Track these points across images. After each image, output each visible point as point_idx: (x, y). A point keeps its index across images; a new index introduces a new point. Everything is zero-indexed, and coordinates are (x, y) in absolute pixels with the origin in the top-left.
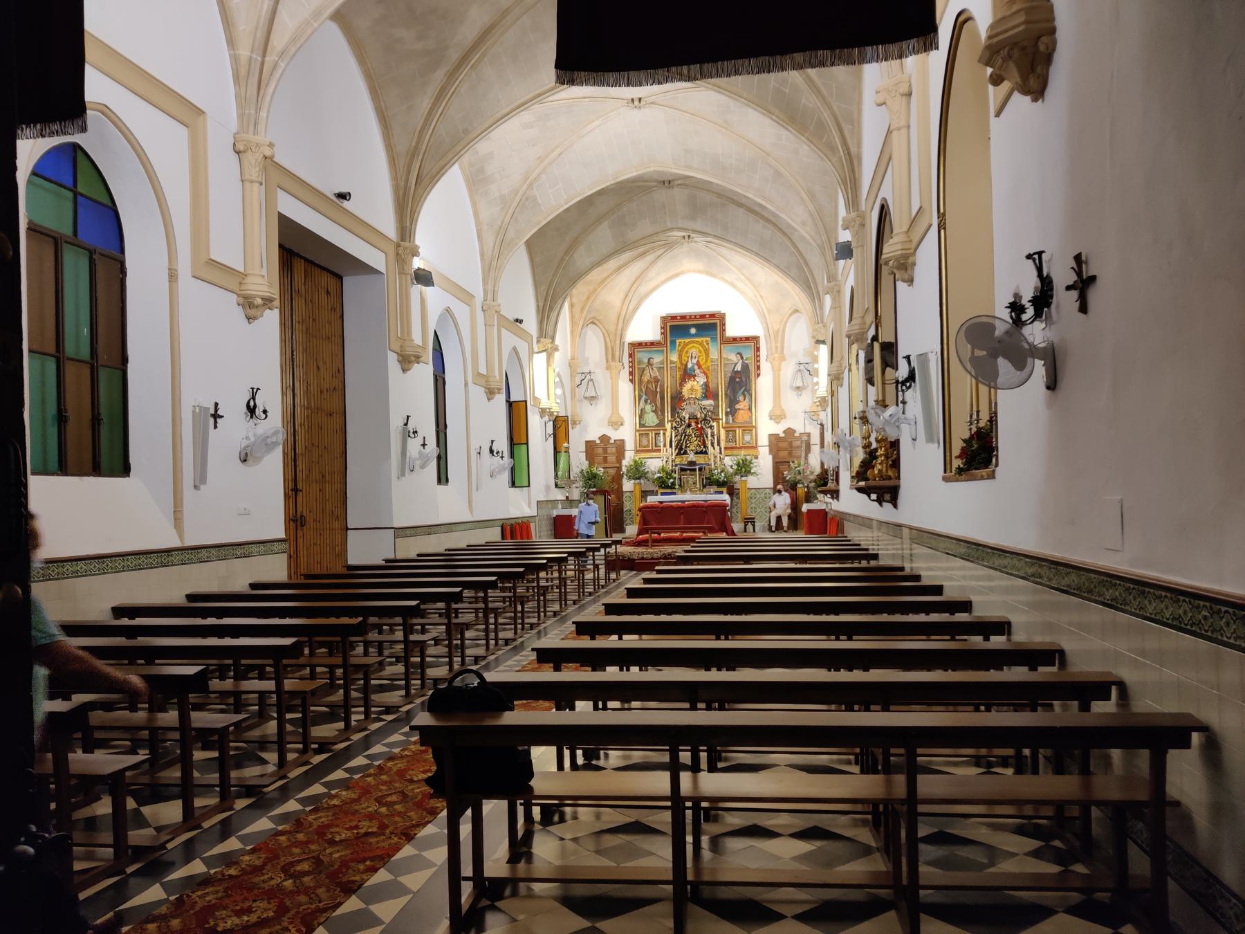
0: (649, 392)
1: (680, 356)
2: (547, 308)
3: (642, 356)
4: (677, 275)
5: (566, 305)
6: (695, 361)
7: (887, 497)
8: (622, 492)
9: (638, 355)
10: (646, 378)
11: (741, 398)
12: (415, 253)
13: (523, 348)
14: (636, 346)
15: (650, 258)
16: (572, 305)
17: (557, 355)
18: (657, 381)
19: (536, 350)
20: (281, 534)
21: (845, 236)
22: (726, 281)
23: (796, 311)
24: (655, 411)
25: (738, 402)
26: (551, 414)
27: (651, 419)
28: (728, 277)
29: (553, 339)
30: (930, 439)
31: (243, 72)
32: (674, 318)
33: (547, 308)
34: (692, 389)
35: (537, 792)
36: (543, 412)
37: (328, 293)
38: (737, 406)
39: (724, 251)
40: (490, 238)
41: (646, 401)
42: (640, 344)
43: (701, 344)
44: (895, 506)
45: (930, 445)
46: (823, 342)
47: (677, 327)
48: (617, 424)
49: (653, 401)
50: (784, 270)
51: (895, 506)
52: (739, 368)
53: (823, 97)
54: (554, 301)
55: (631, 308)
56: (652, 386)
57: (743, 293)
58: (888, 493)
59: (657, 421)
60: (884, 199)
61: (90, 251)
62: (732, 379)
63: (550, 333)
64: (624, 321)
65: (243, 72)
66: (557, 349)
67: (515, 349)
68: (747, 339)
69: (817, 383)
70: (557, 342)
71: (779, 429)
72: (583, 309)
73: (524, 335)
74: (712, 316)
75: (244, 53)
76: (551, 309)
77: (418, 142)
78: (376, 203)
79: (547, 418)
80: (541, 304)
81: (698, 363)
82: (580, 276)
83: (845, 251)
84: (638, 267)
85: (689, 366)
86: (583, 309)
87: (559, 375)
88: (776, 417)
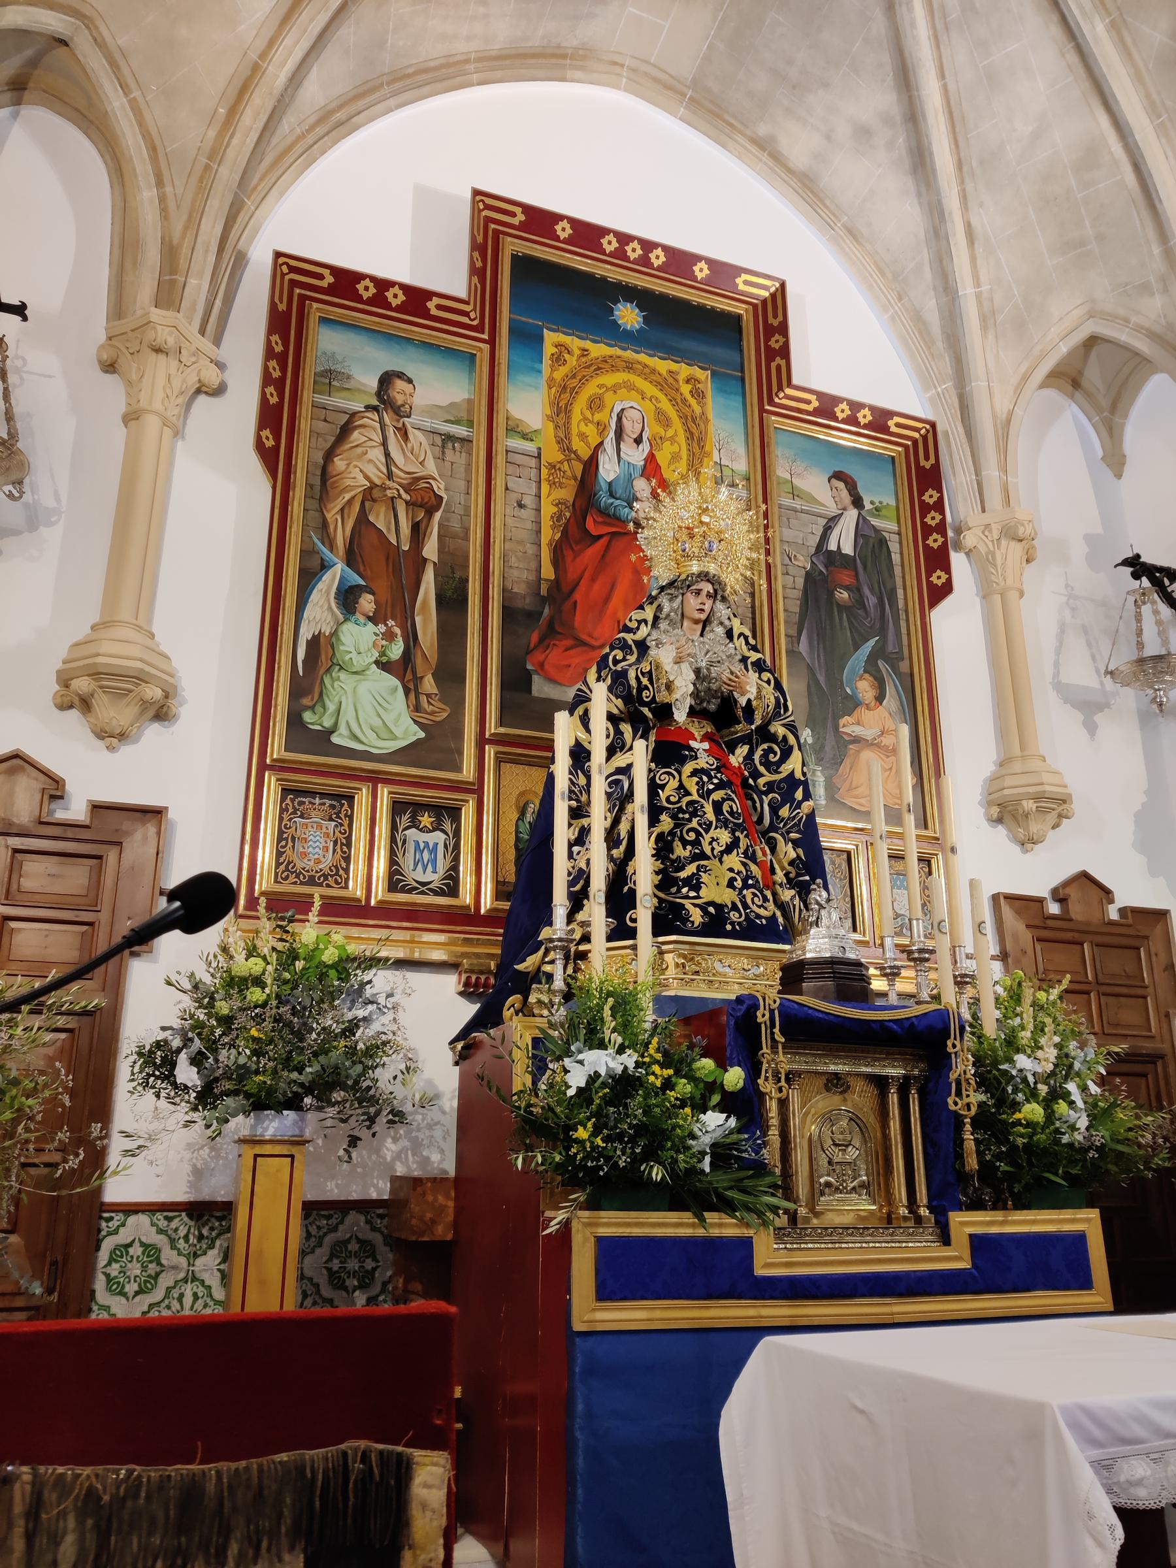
0: (340, 542)
1: (560, 412)
3: (353, 357)
6: (636, 456)
8: (95, 1210)
9: (328, 343)
10: (360, 467)
11: (865, 688)
14: (311, 295)
18: (425, 502)
24: (403, 669)
25: (852, 704)
27: (371, 710)
28: (799, 145)
32: (540, 221)
34: (843, 411)
35: (450, 982)
38: (849, 726)
41: (347, 598)
42: (345, 282)
43: (667, 385)
47: (544, 277)
48: (115, 691)
49: (397, 609)
52: (844, 540)
56: (394, 525)
59: (408, 732)
61: (198, 391)
62: (817, 587)
71: (1038, 874)
81: (651, 468)
85: (608, 470)
88: (1023, 811)
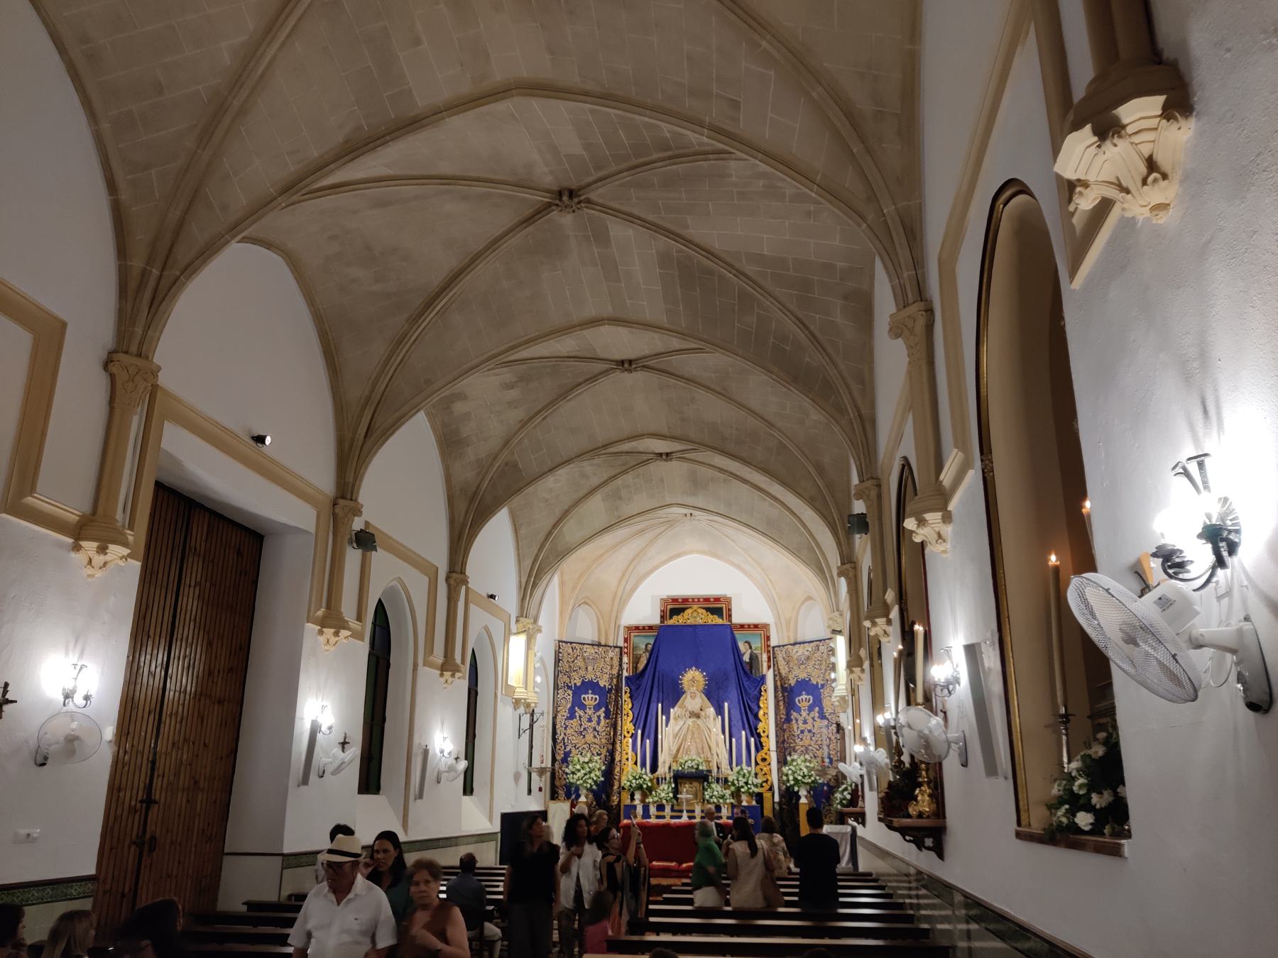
2: (531, 581)
4: (679, 555)
5: (556, 579)
7: (929, 842)
12: (358, 512)
13: (497, 627)
15: (649, 536)
16: (562, 584)
17: (539, 637)
19: (514, 628)
20: (91, 870)
21: (859, 507)
22: (732, 564)
23: (809, 598)
26: (528, 705)
29: (536, 620)
30: (991, 769)
31: (133, 285)
32: (675, 600)
33: (531, 581)
36: (517, 703)
37: (239, 553)
39: (730, 532)
40: (462, 506)
42: (637, 628)
44: (941, 855)
45: (993, 779)
46: (840, 632)
50: (795, 551)
51: (941, 855)
53: (828, 355)
54: (539, 576)
55: (628, 588)
57: (750, 576)
58: (931, 834)
60: (905, 458)
63: (532, 612)
64: (621, 601)
65: (133, 285)
66: (540, 631)
67: (486, 629)
68: (756, 626)
69: (834, 680)
70: (541, 622)
72: (574, 588)
73: (497, 612)
74: (717, 600)
75: (137, 263)
76: (535, 585)
77: (372, 391)
78: (307, 447)
79: (522, 710)
80: (524, 581)
82: (568, 551)
83: (861, 524)
84: (636, 544)
86: (574, 588)
87: (542, 660)
